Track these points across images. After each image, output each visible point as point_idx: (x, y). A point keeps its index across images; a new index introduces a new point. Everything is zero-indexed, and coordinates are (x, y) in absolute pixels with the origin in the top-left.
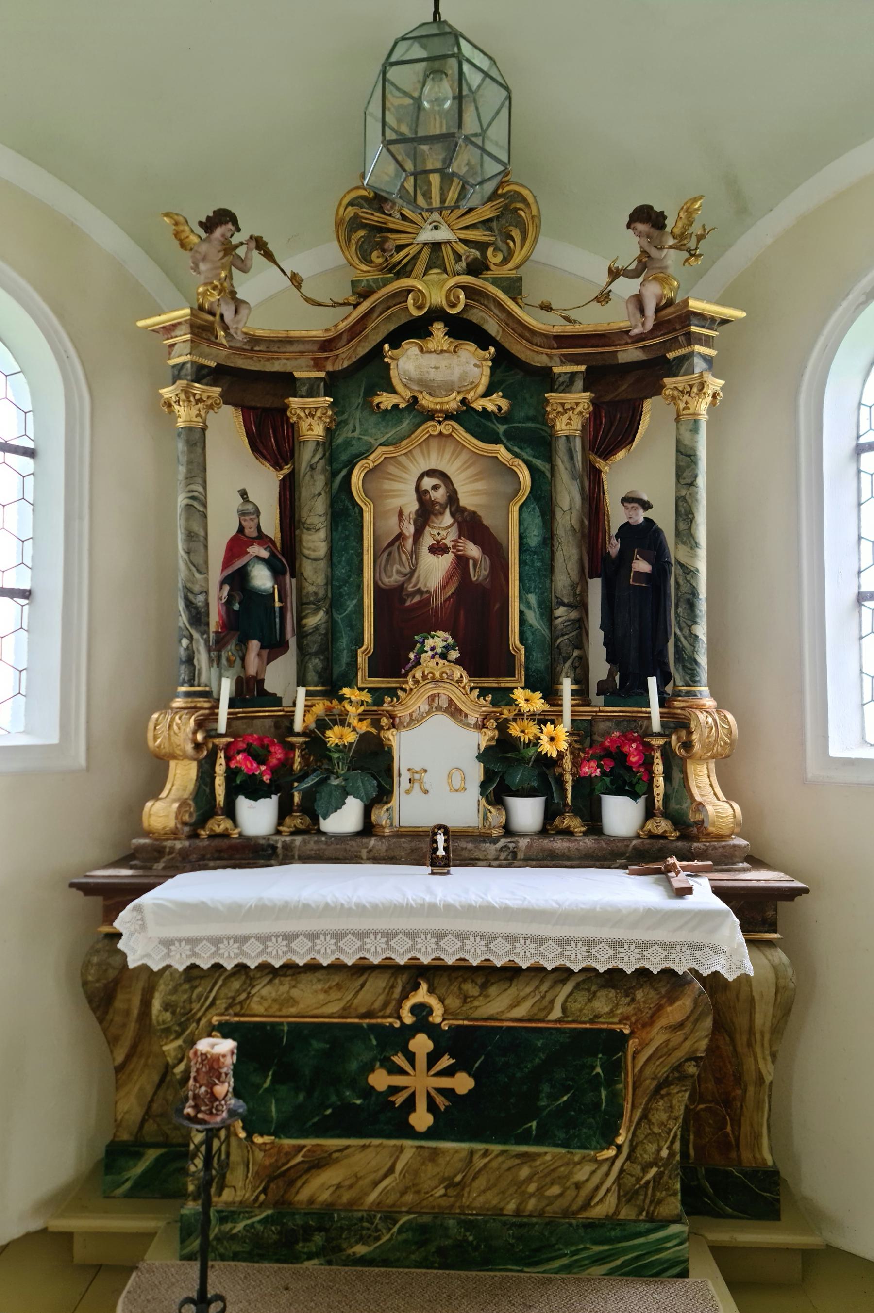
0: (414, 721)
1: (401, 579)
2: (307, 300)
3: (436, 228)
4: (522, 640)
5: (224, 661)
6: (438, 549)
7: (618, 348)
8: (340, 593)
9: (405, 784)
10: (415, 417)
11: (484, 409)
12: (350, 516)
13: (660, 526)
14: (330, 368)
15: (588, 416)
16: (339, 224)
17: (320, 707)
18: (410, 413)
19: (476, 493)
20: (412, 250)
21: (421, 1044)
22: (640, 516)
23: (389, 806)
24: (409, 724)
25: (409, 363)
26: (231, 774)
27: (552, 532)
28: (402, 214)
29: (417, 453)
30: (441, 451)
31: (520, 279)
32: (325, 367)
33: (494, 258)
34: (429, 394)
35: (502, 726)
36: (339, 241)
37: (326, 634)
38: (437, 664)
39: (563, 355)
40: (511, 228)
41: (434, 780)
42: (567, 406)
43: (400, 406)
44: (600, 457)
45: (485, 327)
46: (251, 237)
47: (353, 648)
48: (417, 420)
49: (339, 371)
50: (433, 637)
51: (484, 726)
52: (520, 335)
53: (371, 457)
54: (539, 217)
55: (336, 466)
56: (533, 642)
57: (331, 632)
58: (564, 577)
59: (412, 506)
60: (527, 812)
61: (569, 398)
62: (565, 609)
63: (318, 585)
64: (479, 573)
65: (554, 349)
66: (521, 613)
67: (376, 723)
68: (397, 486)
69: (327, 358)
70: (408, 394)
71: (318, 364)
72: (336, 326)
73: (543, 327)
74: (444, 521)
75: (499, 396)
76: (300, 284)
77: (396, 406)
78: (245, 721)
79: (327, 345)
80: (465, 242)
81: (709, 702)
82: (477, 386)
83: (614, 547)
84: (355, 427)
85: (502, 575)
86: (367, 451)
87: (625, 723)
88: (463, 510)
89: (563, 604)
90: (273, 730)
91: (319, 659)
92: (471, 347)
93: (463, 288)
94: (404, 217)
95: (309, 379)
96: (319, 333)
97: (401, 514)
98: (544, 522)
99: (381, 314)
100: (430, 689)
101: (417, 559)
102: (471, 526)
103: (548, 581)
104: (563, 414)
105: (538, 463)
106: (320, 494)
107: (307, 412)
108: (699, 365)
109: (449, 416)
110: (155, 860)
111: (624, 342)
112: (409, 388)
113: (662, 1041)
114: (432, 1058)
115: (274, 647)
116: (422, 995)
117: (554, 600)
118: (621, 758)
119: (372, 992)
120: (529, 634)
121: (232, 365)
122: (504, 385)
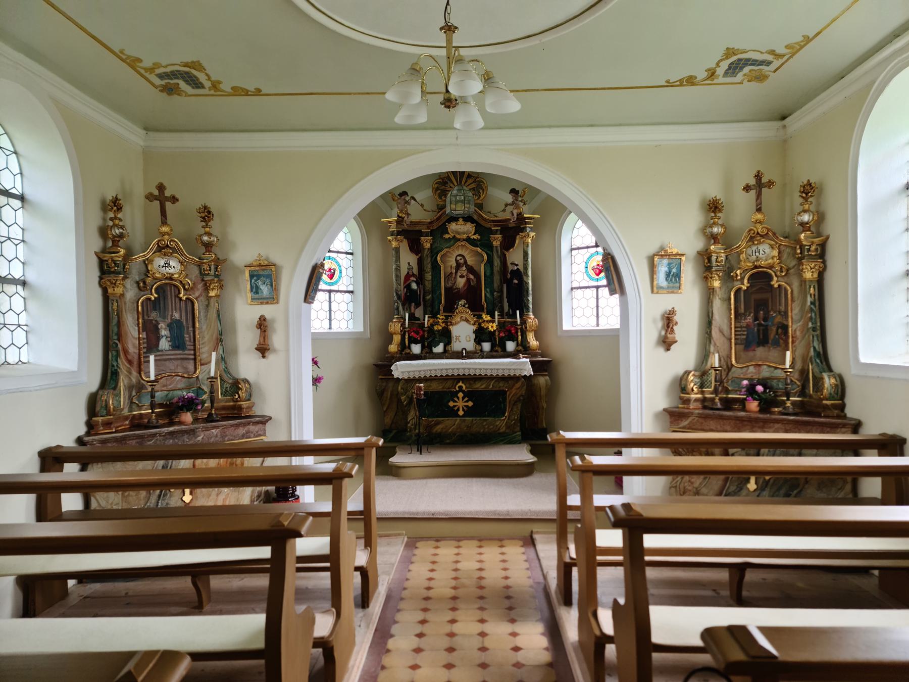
0: (456, 323)
6: (462, 276)
17: (431, 321)
21: (461, 395)
22: (516, 268)
25: (453, 226)
26: (409, 338)
35: (480, 324)
41: (462, 339)
57: (433, 300)
58: (496, 284)
59: (454, 265)
60: (487, 346)
61: (496, 236)
79: (430, 223)
81: (532, 316)
83: (509, 276)
100: (461, 315)
102: (471, 270)
108: (528, 230)
110: (394, 358)
113: (514, 392)
114: (463, 398)
115: (418, 305)
116: (460, 384)
118: (510, 331)
119: (449, 384)
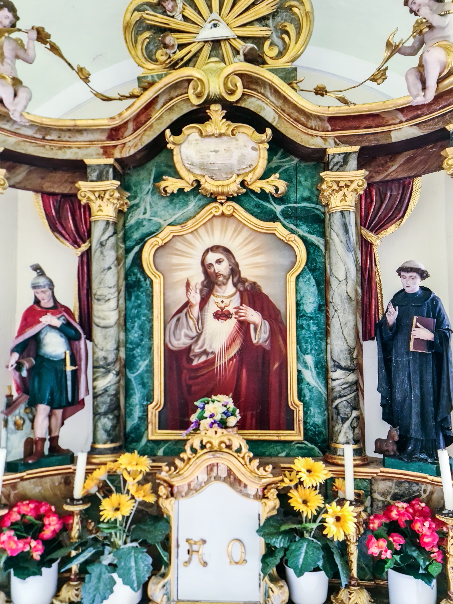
0: (192, 490)
1: (188, 342)
2: (97, 95)
3: (215, 25)
4: (301, 396)
5: (11, 425)
6: (222, 315)
7: (392, 127)
8: (133, 355)
9: (183, 556)
10: (200, 200)
11: (262, 190)
12: (142, 287)
13: (436, 295)
14: (118, 155)
15: (362, 192)
16: (126, 28)
18: (195, 196)
19: (257, 266)
20: (194, 48)
22: (414, 285)
23: (165, 580)
24: (187, 494)
25: (192, 150)
27: (326, 300)
28: (183, 16)
29: (202, 231)
30: (224, 230)
31: (295, 69)
32: (113, 154)
33: (269, 52)
34: (211, 177)
35: (283, 496)
36: (126, 42)
37: (117, 395)
38: (216, 432)
39: (336, 137)
40: (286, 24)
42: (342, 184)
43: (186, 190)
44: (371, 231)
45: (262, 114)
46: (33, 28)
47: (145, 403)
48: (202, 203)
49: (126, 158)
50: (213, 402)
51: (264, 497)
52: (295, 120)
53: (161, 236)
54: (313, 13)
55: (129, 243)
56: (310, 399)
58: (339, 345)
59: (198, 278)
62: (343, 372)
63: (107, 351)
64: (261, 336)
65: (328, 131)
66: (299, 372)
67: (155, 490)
68: (183, 260)
69: (115, 146)
70: (190, 178)
71: (107, 151)
72: (120, 114)
73: (318, 109)
74: (227, 291)
75: (276, 178)
76: (87, 78)
77: (181, 191)
78: (32, 480)
79: (115, 133)
80: (244, 39)
82: (254, 169)
84: (146, 209)
85: (280, 338)
86: (157, 230)
87: (407, 485)
88: (243, 281)
89: (340, 367)
90: (62, 486)
91: (108, 418)
92: (249, 130)
93: (241, 76)
94: (185, 18)
95: (99, 165)
96: (105, 122)
97: (188, 285)
98: (320, 291)
99: (164, 104)
100: (209, 459)
101: (202, 324)
102: (253, 296)
103: (324, 344)
104: (337, 192)
105: (314, 239)
106: (110, 268)
107: (97, 194)
109: (230, 198)
111: (398, 121)
112: (192, 173)
117: (330, 364)
118: (413, 538)
120: (306, 391)
121: (23, 152)
122: (281, 170)
